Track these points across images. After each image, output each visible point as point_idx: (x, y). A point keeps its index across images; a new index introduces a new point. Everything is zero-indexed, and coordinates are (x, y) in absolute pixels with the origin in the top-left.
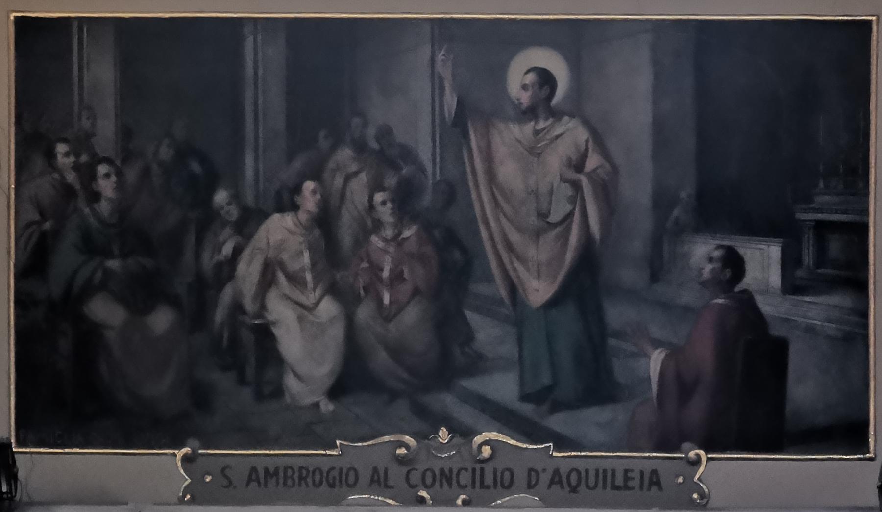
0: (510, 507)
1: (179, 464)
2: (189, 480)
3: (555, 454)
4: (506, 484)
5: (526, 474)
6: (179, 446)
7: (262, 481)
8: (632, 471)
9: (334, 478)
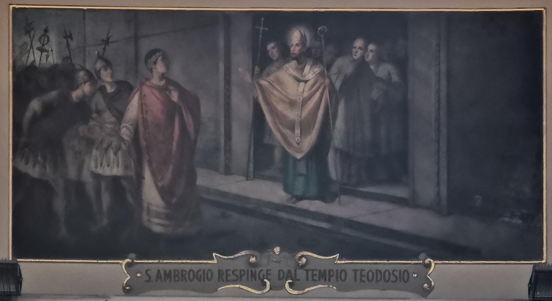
0: (283, 298)
1: (124, 267)
2: (129, 278)
3: (339, 262)
4: (387, 279)
5: (277, 272)
6: (123, 258)
7: (163, 279)
8: (229, 270)
9: (264, 275)
